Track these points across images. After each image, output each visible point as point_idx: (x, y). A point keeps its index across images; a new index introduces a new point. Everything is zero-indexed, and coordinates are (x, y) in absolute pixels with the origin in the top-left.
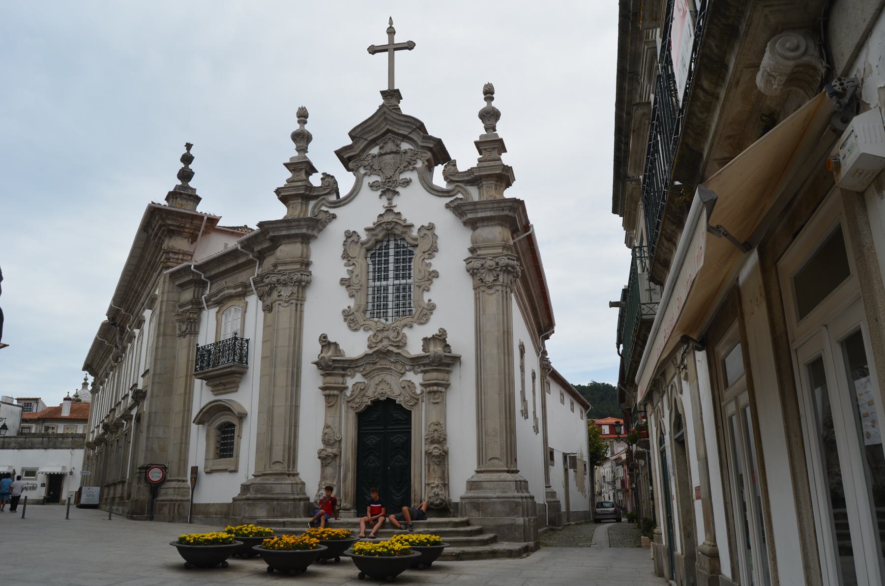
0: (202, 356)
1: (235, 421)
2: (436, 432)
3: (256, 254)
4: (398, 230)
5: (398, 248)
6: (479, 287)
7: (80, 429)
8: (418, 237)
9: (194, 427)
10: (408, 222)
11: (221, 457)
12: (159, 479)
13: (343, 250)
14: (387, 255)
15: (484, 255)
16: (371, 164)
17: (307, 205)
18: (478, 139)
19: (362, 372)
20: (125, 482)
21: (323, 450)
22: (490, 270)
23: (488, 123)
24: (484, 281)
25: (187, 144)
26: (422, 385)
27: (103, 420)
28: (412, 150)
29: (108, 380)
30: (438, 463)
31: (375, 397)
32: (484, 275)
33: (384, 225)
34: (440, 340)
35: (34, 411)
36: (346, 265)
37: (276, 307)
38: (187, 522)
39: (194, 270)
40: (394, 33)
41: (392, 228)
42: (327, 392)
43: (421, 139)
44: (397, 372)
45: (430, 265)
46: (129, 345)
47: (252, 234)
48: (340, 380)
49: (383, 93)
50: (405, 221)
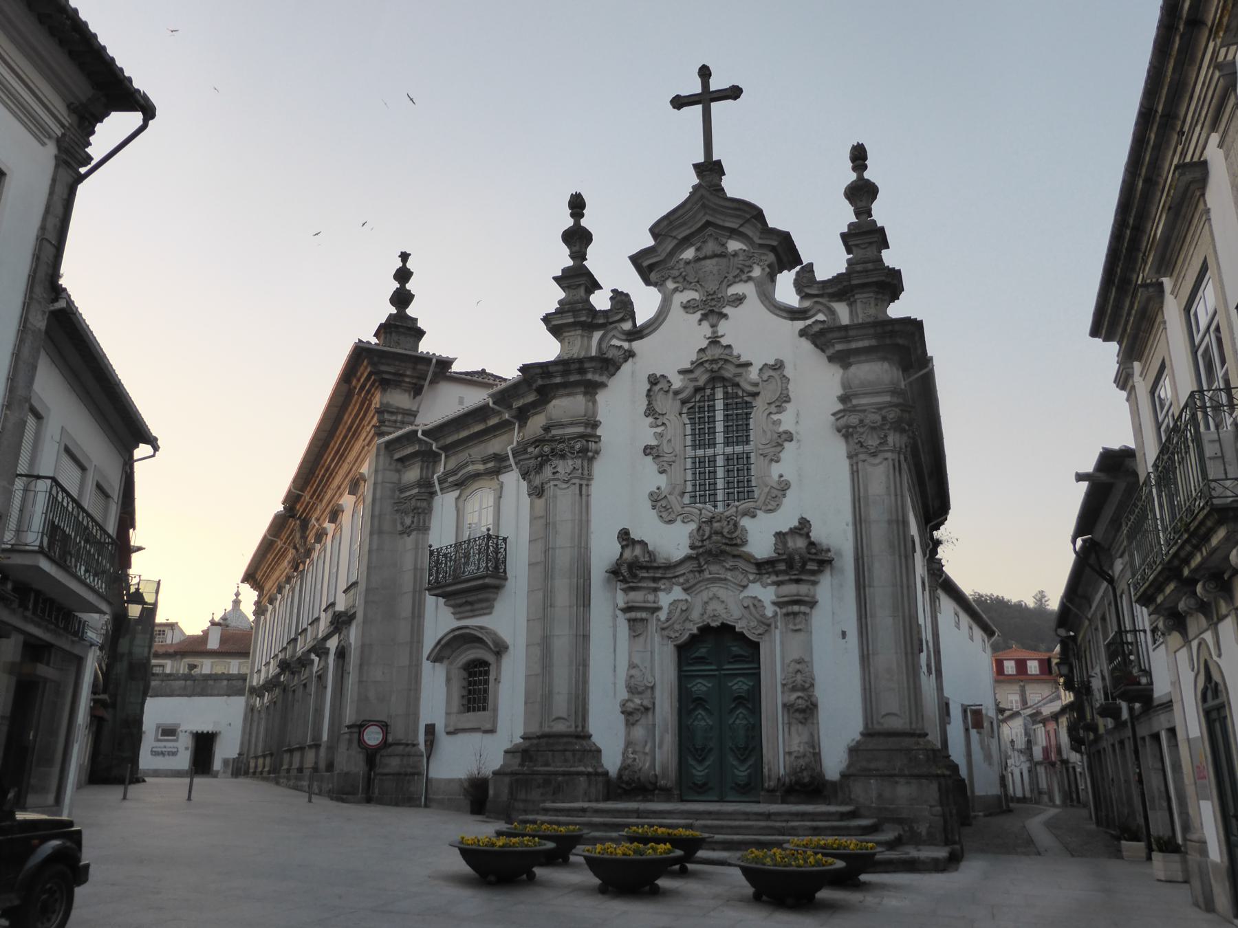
0: (438, 563)
1: (490, 658)
2: (799, 674)
3: (514, 412)
4: (729, 372)
5: (727, 399)
6: (857, 455)
7: (234, 666)
8: (760, 381)
9: (427, 666)
10: (743, 359)
11: (469, 710)
12: (377, 742)
13: (647, 403)
14: (712, 409)
15: (863, 405)
16: (684, 274)
17: (590, 338)
18: (846, 230)
19: (682, 584)
20: (320, 745)
21: (627, 701)
22: (873, 429)
23: (860, 204)
24: (864, 444)
25: (402, 253)
26: (774, 603)
27: (276, 656)
28: (745, 250)
29: (283, 597)
30: (803, 721)
31: (703, 621)
32: (864, 436)
33: (707, 365)
34: (801, 535)
35: (169, 641)
36: (651, 427)
37: (550, 489)
38: (419, 806)
39: (422, 437)
40: (710, 75)
41: (719, 368)
42: (633, 615)
43: (758, 234)
44: (735, 583)
45: (779, 422)
46: (318, 546)
47: (504, 385)
48: (651, 597)
49: (696, 166)
50: (738, 357)
